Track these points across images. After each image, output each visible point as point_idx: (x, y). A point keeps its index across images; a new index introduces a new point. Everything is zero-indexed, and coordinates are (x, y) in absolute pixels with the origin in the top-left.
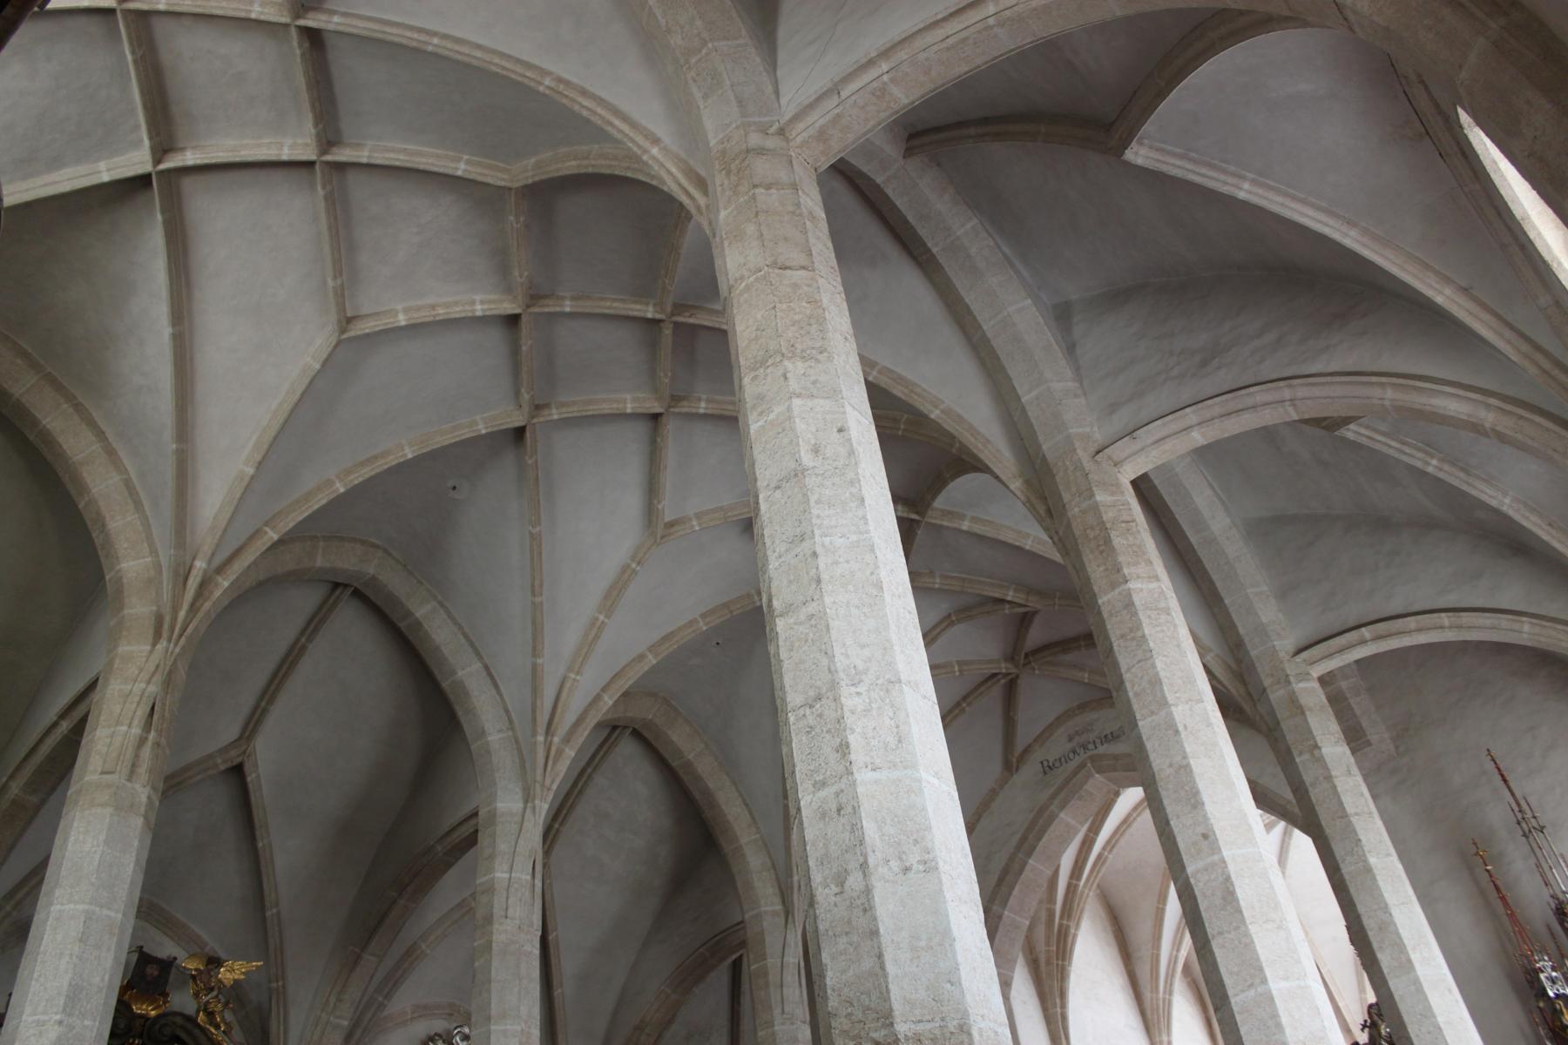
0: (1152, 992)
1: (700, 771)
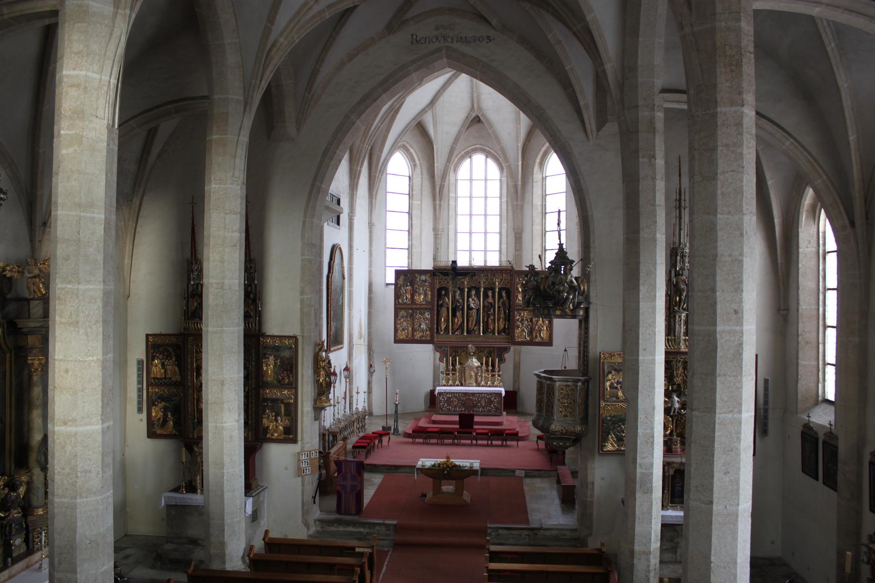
0: (361, 142)
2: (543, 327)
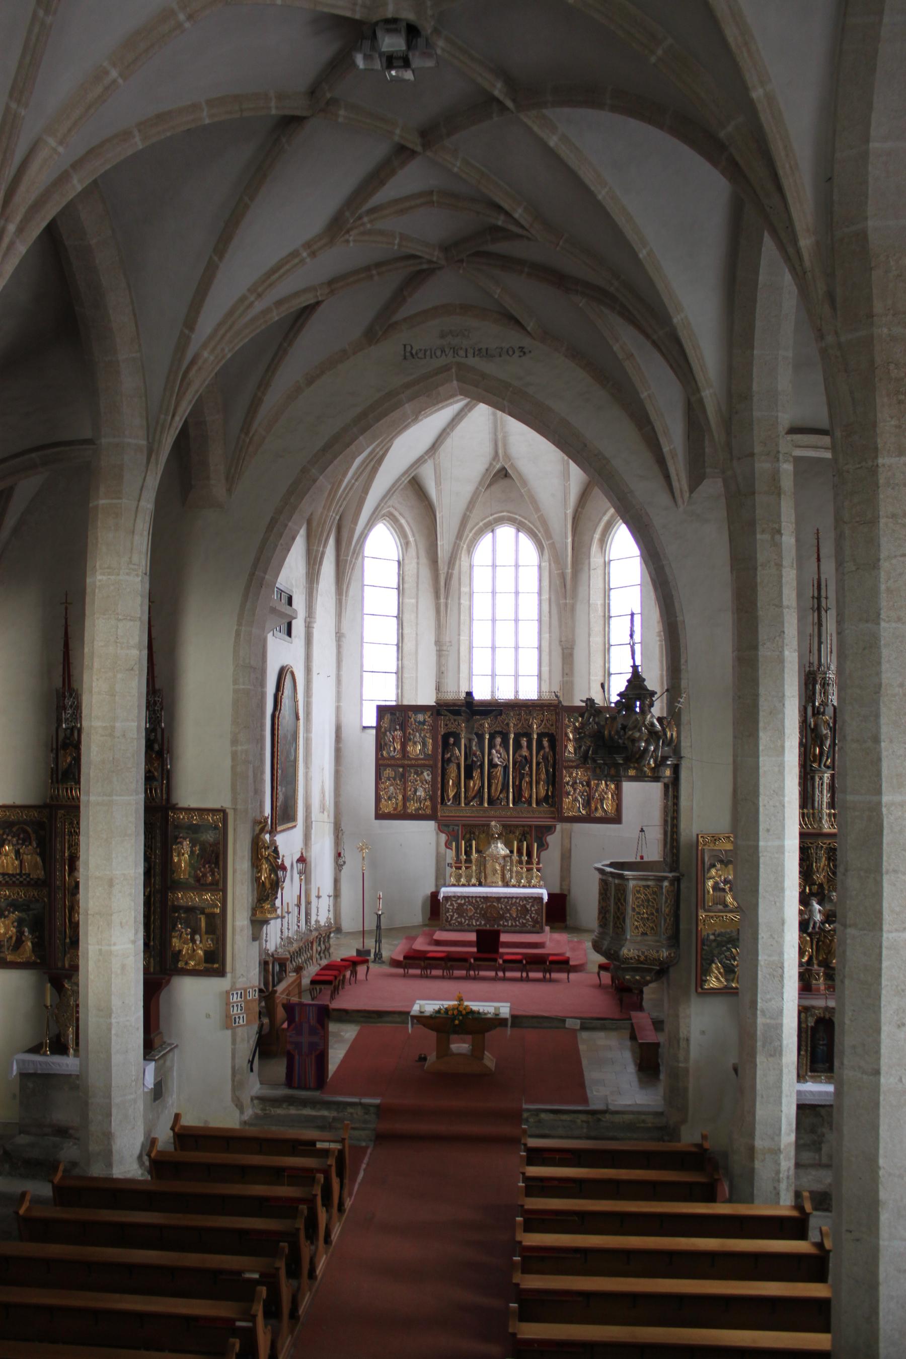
0: (324, 508)
2: (606, 793)
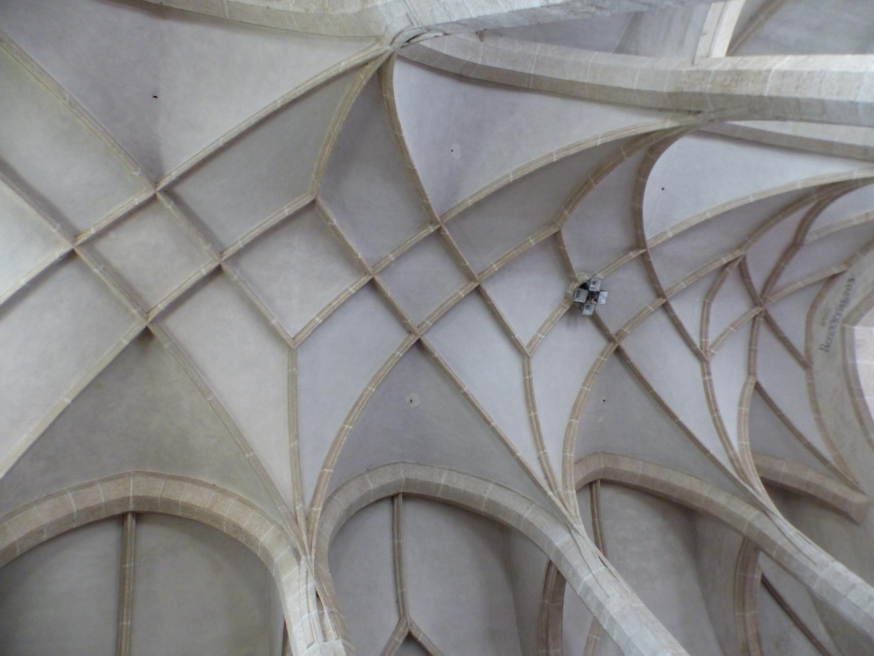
1: (651, 476)
